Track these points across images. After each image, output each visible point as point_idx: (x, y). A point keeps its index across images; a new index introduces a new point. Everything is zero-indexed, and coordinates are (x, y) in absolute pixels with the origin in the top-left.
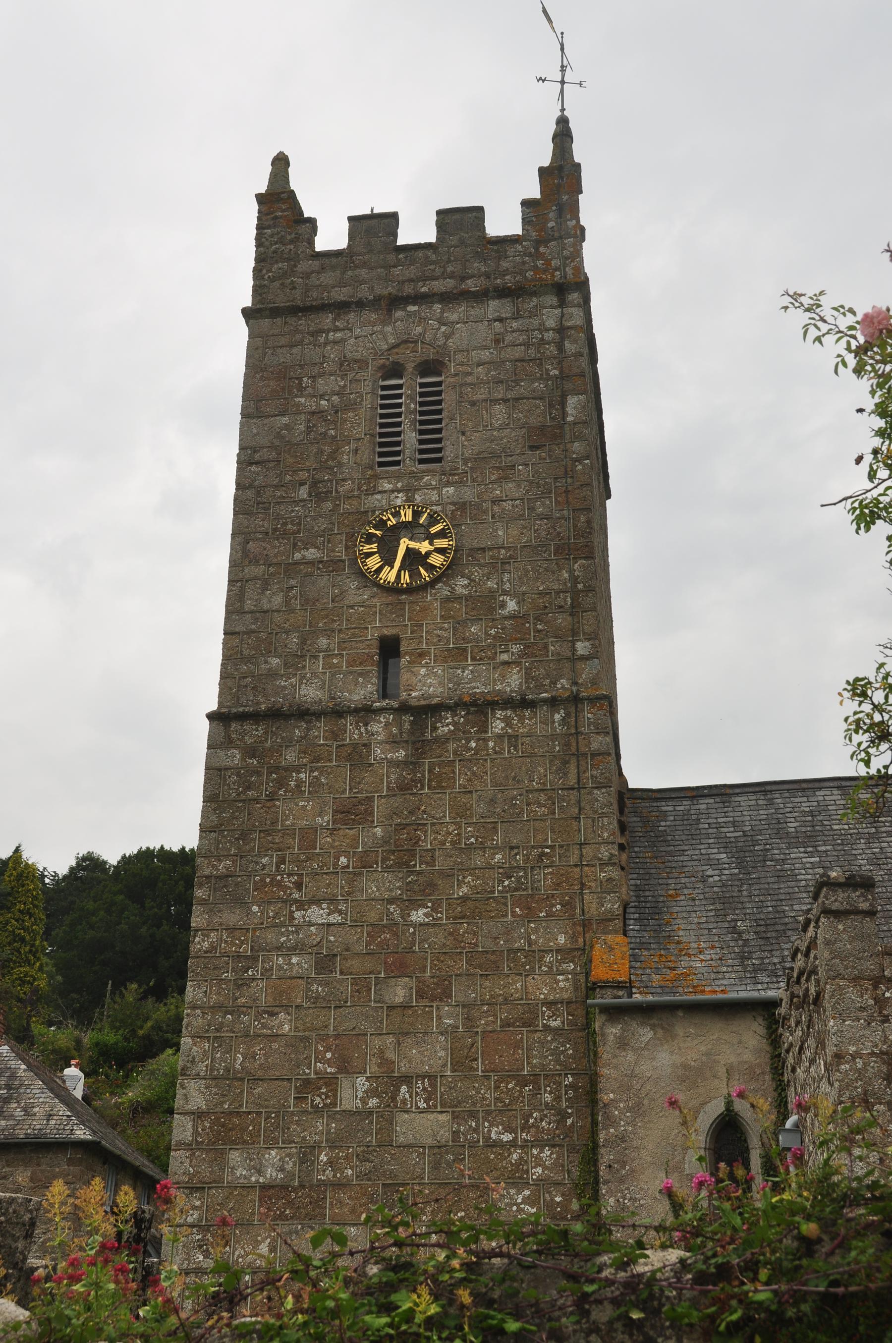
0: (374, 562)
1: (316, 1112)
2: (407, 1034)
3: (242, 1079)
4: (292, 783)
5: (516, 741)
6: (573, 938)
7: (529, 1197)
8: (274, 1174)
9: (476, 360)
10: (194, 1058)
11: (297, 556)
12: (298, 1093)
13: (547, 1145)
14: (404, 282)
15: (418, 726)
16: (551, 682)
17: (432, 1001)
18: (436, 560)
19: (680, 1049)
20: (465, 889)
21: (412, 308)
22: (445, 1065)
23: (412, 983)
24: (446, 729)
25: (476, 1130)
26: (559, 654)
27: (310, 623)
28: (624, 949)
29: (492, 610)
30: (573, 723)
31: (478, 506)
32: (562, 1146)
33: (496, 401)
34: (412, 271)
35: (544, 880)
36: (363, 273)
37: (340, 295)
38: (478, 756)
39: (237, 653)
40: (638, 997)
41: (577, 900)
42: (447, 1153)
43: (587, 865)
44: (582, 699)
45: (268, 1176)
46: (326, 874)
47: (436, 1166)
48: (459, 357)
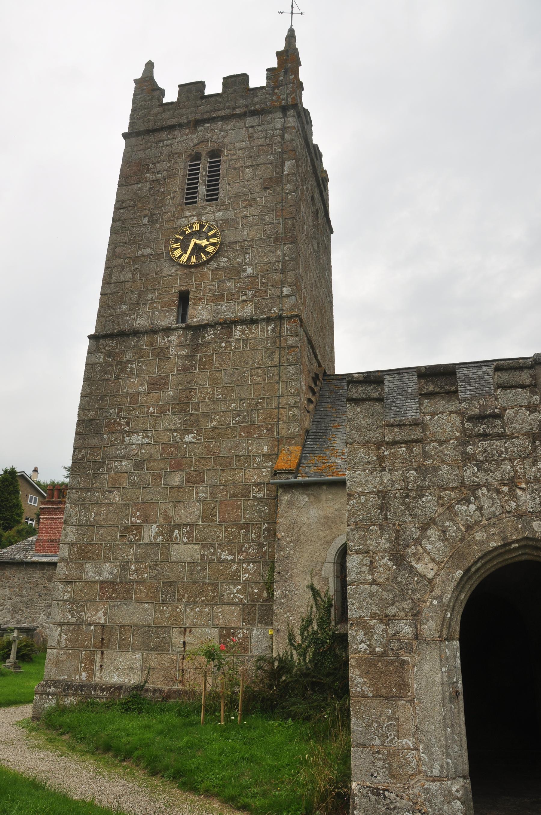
0: (178, 253)
1: (130, 543)
2: (179, 502)
3: (93, 526)
4: (128, 370)
5: (247, 342)
6: (272, 448)
7: (240, 590)
8: (107, 576)
9: (238, 147)
10: (71, 515)
11: (140, 253)
12: (121, 533)
13: (251, 562)
14: (204, 113)
15: (195, 336)
16: (269, 310)
17: (194, 484)
18: (210, 249)
19: (323, 507)
20: (215, 423)
21: (207, 125)
22: (198, 519)
23: (184, 474)
24: (210, 337)
25: (213, 554)
26: (273, 295)
27: (144, 286)
28: (298, 453)
29: (239, 273)
30: (278, 331)
31: (234, 220)
32: (259, 562)
33: (247, 167)
34: (208, 108)
35: (258, 417)
36: (184, 111)
37: (170, 122)
38: (226, 351)
39: (106, 304)
40: (300, 479)
41: (275, 427)
42: (197, 566)
43: (282, 408)
44: (284, 318)
45: (104, 577)
46: (142, 417)
47: (191, 573)
48: (230, 147)
